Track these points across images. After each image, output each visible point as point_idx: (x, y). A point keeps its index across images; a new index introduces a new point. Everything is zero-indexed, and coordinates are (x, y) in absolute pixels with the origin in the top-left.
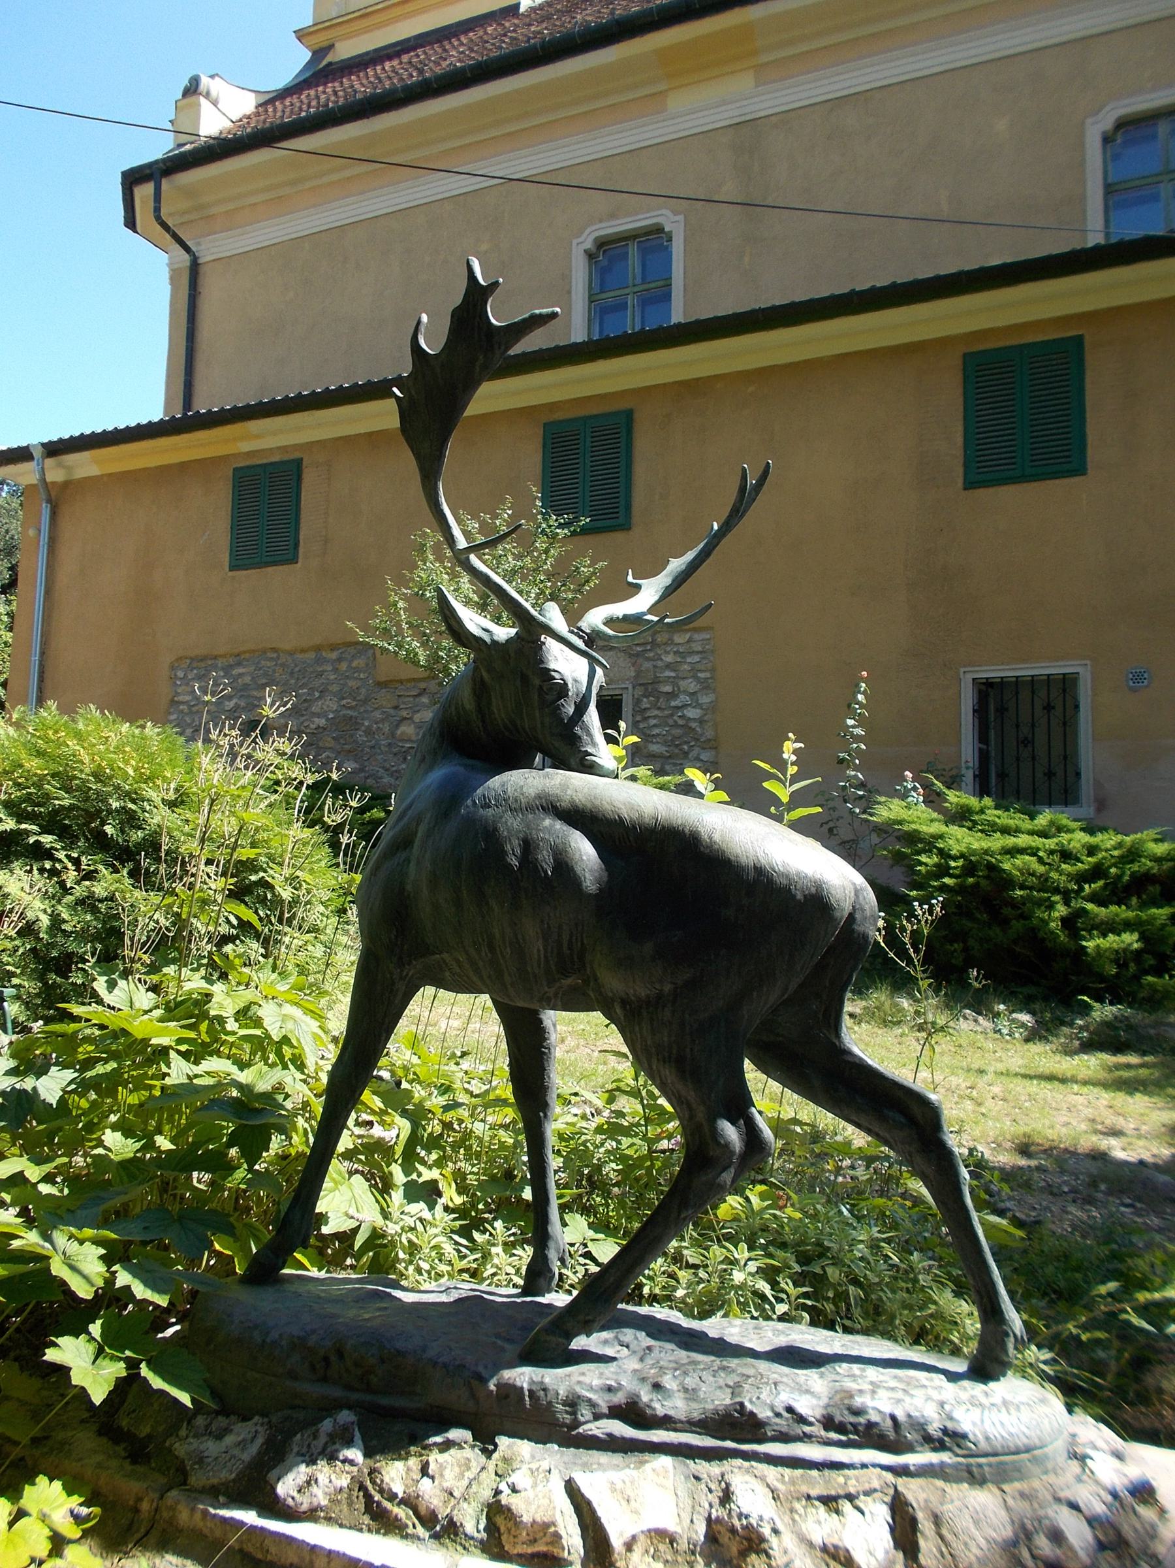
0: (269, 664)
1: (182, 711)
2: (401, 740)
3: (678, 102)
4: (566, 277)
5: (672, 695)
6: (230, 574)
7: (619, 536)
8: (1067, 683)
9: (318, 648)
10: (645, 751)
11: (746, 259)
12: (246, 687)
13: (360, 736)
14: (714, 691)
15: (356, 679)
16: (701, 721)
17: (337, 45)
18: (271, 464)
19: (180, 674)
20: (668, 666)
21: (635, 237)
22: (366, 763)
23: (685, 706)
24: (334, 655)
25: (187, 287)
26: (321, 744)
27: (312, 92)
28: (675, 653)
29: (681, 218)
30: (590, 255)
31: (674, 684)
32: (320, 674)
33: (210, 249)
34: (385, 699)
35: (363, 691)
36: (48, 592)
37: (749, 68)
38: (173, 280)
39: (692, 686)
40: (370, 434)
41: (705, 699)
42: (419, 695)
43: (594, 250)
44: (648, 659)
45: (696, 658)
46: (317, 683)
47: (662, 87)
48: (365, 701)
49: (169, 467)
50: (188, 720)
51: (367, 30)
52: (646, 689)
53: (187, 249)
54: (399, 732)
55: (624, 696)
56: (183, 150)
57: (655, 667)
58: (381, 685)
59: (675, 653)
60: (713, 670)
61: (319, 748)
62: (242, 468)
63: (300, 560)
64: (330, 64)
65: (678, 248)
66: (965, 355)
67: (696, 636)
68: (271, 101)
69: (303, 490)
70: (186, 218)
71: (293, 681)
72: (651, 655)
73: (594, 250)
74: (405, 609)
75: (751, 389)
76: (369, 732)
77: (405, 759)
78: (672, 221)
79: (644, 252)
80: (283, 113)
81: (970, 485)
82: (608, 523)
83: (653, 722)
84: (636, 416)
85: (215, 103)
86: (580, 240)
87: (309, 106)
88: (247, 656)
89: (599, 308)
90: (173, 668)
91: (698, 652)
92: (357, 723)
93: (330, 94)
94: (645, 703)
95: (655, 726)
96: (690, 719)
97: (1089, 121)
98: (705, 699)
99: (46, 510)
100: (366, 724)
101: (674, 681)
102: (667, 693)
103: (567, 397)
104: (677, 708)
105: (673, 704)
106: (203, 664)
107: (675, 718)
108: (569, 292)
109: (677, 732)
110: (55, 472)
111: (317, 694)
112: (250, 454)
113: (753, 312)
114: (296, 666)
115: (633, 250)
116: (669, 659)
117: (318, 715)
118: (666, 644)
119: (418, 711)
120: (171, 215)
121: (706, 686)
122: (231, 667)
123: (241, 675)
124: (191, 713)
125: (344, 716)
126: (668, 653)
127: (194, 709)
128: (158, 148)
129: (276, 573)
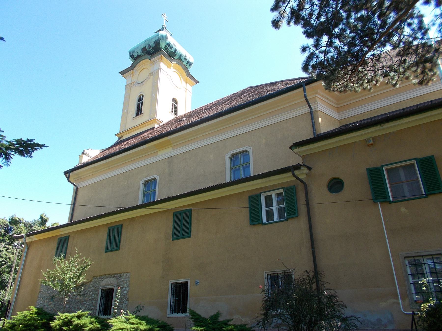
3: (160, 153)
7: (117, 251)
8: (187, 283)
11: (169, 184)
16: (126, 294)
20: (122, 281)
21: (152, 180)
29: (158, 176)
30: (230, 158)
33: (80, 185)
41: (128, 289)
43: (145, 183)
44: (119, 280)
45: (127, 279)
47: (157, 150)
51: (135, 130)
62: (60, 238)
64: (121, 140)
66: (174, 212)
70: (77, 179)
73: (231, 157)
75: (141, 219)
81: (173, 240)
82: (115, 249)
87: (177, 124)
89: (145, 195)
97: (226, 155)
108: (139, 192)
110: (28, 240)
116: (123, 279)
126: (122, 278)
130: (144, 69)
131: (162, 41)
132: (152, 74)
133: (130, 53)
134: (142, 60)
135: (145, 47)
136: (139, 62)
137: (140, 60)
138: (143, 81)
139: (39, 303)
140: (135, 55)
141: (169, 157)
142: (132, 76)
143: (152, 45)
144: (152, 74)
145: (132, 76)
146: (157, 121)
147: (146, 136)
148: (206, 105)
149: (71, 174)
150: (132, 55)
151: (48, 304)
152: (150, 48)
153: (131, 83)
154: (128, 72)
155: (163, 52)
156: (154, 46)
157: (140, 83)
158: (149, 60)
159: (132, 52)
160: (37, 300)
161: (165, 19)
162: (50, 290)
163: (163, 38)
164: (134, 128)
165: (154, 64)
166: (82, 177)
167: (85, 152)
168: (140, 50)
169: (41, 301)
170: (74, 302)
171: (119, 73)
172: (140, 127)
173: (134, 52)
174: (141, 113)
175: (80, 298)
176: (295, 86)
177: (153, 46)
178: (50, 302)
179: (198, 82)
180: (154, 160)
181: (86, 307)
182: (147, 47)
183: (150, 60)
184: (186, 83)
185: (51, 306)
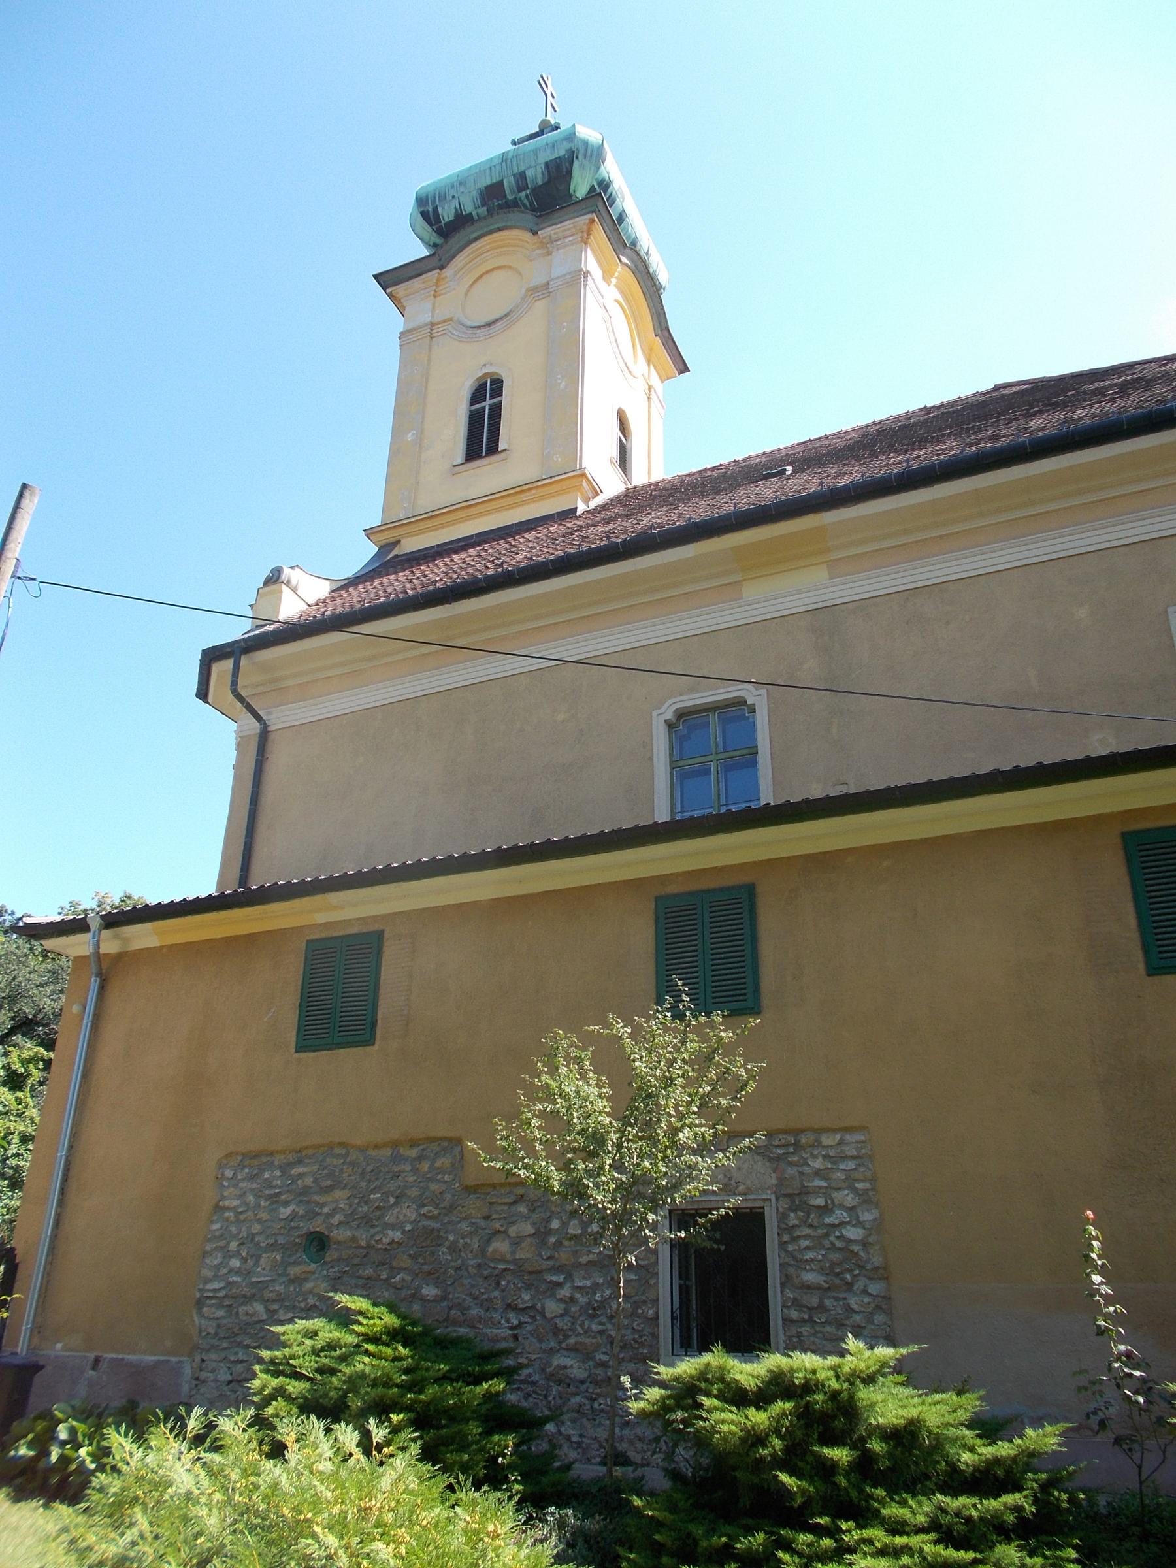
0: (335, 1162)
1: (227, 1219)
2: (493, 1260)
3: (751, 591)
4: (647, 745)
5: (826, 1210)
6: (297, 1055)
9: (395, 1144)
10: (797, 1281)
11: (834, 731)
12: (306, 1191)
13: (443, 1254)
14: (877, 1205)
15: (439, 1181)
16: (864, 1244)
17: (403, 541)
18: (349, 935)
19: (229, 1173)
20: (817, 1173)
21: (718, 708)
22: (450, 1289)
23: (843, 1224)
24: (413, 1153)
25: (255, 753)
26: (395, 1264)
27: (385, 580)
28: (824, 1157)
30: (670, 725)
31: (827, 1196)
32: (396, 1176)
33: (278, 719)
34: (473, 1207)
35: (448, 1196)
36: (86, 1075)
37: (823, 563)
38: (239, 746)
39: (850, 1199)
40: (459, 906)
41: (867, 1216)
42: (515, 1202)
44: (791, 1164)
45: (851, 1165)
46: (392, 1186)
48: (451, 1208)
49: (235, 939)
50: (233, 1229)
51: (431, 529)
52: (793, 1202)
53: (258, 718)
54: (490, 1249)
55: (767, 1209)
56: (262, 630)
57: (801, 1173)
58: (470, 1190)
59: (824, 1157)
60: (873, 1180)
61: (392, 1268)
63: (377, 1042)
64: (396, 556)
65: (762, 719)
67: (848, 1138)
68: (345, 587)
69: (383, 963)
70: (260, 689)
71: (363, 1184)
72: (796, 1159)
74: (540, 1128)
75: (885, 864)
76: (453, 1248)
77: (498, 1284)
78: (751, 694)
79: (724, 721)
80: (356, 598)
83: (804, 1243)
84: (759, 890)
85: (294, 590)
86: (659, 711)
88: (310, 1152)
90: (220, 1165)
91: (853, 1158)
92: (439, 1237)
93: (398, 584)
94: (793, 1219)
95: (807, 1248)
96: (850, 1241)
98: (867, 1216)
99: (94, 983)
100: (451, 1238)
101: (826, 1192)
102: (819, 1207)
103: (680, 870)
104: (833, 1226)
105: (827, 1220)
106: (256, 1162)
107: (832, 1238)
108: (651, 759)
109: (836, 1256)
110: (110, 944)
111: (392, 1200)
112: (327, 925)
113: (888, 789)
114: (368, 1165)
115: (714, 720)
116: (818, 1164)
117: (393, 1227)
118: (812, 1146)
119: (514, 1223)
120: (244, 687)
121: (866, 1199)
122: (291, 1165)
123: (301, 1176)
124: (238, 1221)
125: (424, 1227)
127: (242, 1217)
128: (236, 630)
129: (347, 1056)
130: (495, 272)
131: (582, 166)
132: (542, 290)
133: (421, 201)
134: (491, 232)
135: (501, 183)
136: (476, 239)
137: (479, 233)
138: (501, 319)
139: (217, 1267)
140: (447, 213)
141: (815, 606)
142: (435, 296)
143: (536, 175)
144: (542, 290)
145: (435, 296)
146: (584, 483)
147: (526, 551)
148: (722, 463)
149: (244, 660)
150: (430, 209)
151: (284, 1274)
152: (520, 190)
153: (432, 325)
154: (419, 275)
155: (600, 204)
156: (544, 184)
157: (479, 327)
158: (527, 236)
159: (434, 201)
160: (205, 1254)
161: (550, 98)
162: (286, 1204)
163: (588, 155)
164: (468, 507)
165: (549, 254)
166: (291, 682)
167: (284, 577)
168: (475, 193)
169: (228, 1255)
170: (473, 1271)
171: (375, 277)
172: (494, 505)
173: (443, 197)
174: (493, 449)
175: (514, 1253)
176: (659, 536)
177: (540, 182)
178: (295, 1263)
179: (686, 369)
180: (597, 647)
181: (572, 1299)
182: (509, 183)
183: (535, 233)
184: (649, 362)
185: (309, 1285)
